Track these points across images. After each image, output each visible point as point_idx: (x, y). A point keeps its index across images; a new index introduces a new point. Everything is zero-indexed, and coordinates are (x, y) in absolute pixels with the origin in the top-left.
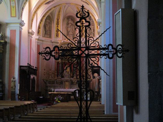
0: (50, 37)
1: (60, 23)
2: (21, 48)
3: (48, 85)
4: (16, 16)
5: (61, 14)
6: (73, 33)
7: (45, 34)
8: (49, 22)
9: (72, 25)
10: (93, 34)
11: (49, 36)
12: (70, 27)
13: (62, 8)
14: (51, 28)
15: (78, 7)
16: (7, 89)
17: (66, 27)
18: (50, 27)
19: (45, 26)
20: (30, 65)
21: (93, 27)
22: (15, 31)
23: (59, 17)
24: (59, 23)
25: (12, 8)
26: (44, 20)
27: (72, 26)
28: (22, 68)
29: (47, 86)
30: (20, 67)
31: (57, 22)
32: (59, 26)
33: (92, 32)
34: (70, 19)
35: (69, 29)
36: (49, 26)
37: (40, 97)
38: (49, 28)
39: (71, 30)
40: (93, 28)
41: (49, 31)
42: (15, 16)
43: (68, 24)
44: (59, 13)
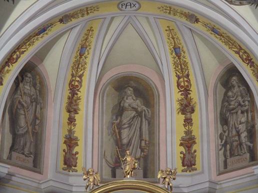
0: (36, 165)
1: (82, 105)
5: (88, 61)
6: (142, 151)
7: (12, 149)
8: (31, 97)
9: (139, 114)
10: (245, 149)
11: (31, 159)
12: (130, 126)
13: (96, 32)
14: (42, 124)
15: (173, 26)
17: (113, 124)
18: (36, 118)
21: (243, 120)
23: (80, 77)
24: (77, 105)
27: (137, 123)
31: (69, 98)
32: (77, 117)
33: (241, 144)
34: (130, 91)
35: (125, 133)
36: (31, 117)
38: (34, 124)
39: (135, 141)
40: (247, 122)
41: (30, 138)
43: (119, 111)
44: (81, 55)
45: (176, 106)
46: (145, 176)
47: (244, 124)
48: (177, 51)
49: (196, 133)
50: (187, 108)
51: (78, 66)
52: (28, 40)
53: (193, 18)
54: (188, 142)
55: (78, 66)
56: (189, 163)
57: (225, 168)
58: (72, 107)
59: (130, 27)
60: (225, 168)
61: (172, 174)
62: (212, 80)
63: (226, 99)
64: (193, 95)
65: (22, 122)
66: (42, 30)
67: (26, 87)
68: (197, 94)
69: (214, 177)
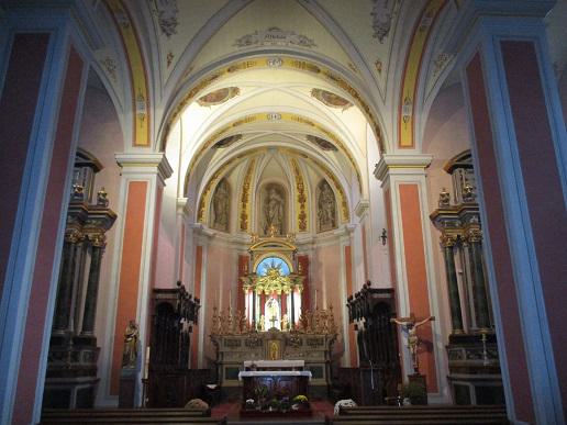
0: (227, 229)
1: (249, 198)
2: (159, 255)
3: (223, 349)
4: (148, 145)
7: (215, 221)
9: (278, 203)
14: (230, 209)
16: (127, 357)
19: (215, 203)
20: (183, 288)
22: (144, 184)
25: (124, 31)
26: (213, 187)
28: (159, 296)
29: (222, 353)
30: (154, 292)
37: (210, 386)
42: (410, 144)
43: (268, 201)
45: (297, 198)
46: (470, 156)
47: (215, 358)
48: (297, 171)
49: (307, 212)
50: (302, 199)
51: (247, 178)
52: (222, 167)
53: (305, 155)
54: (303, 217)
55: (247, 178)
56: (303, 227)
57: (320, 230)
58: (244, 200)
59: (273, 161)
60: (320, 230)
61: (294, 235)
62: (315, 185)
63: (321, 195)
64: (305, 193)
65: (220, 207)
66: (229, 162)
67: (222, 190)
68: (307, 192)
69: (315, 235)
